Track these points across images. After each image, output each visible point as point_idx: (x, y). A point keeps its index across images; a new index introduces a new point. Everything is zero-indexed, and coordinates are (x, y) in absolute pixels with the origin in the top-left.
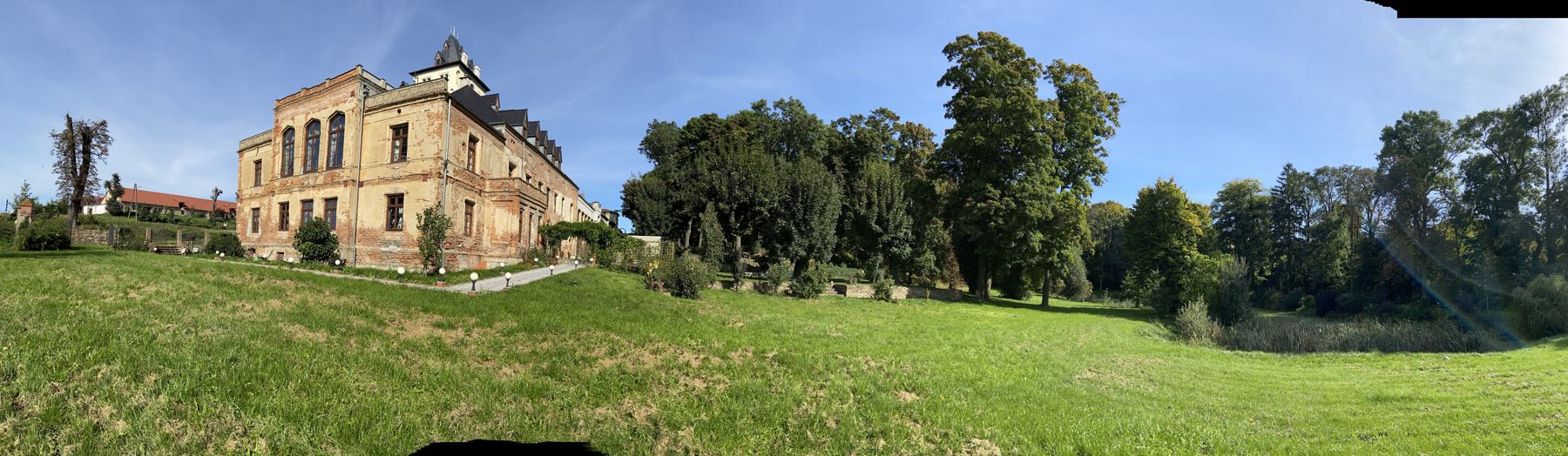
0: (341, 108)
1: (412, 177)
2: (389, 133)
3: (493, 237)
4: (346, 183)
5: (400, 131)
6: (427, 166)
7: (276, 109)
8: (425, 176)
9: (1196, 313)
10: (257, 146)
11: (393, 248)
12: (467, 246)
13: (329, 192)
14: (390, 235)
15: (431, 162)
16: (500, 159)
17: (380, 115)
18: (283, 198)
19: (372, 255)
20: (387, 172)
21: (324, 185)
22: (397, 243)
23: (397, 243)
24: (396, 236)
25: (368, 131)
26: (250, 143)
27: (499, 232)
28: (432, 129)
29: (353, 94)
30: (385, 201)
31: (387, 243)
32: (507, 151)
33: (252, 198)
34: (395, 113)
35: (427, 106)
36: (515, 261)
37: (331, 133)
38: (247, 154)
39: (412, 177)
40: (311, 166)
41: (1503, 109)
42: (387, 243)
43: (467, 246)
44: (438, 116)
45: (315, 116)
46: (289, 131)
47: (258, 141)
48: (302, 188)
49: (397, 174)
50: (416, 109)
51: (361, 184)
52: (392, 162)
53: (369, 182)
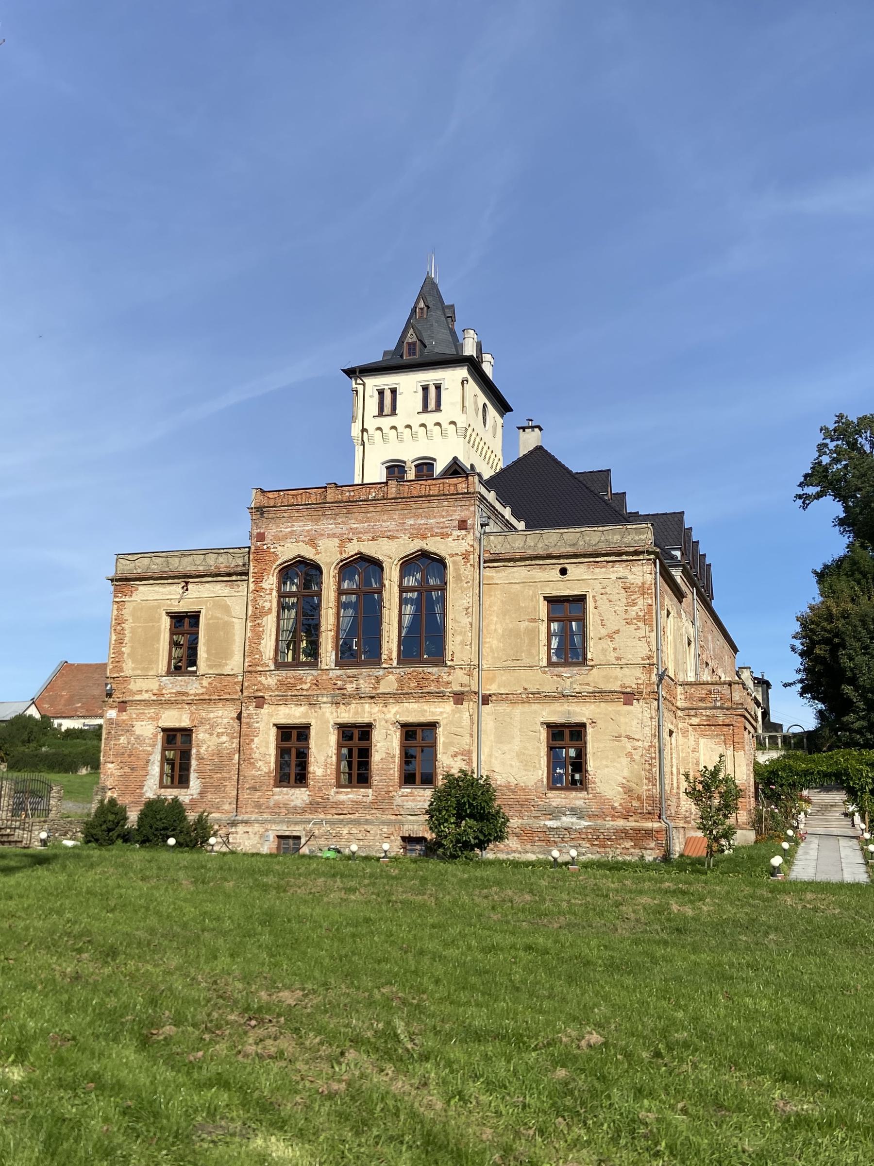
0: (434, 546)
1: (600, 695)
4: (459, 698)
6: (632, 678)
7: (260, 510)
8: (629, 697)
10: (186, 578)
11: (567, 820)
13: (415, 711)
14: (557, 799)
15: (638, 672)
17: (519, 573)
18: (293, 714)
20: (548, 682)
21: (399, 696)
22: (575, 812)
23: (575, 812)
24: (577, 798)
25: (494, 601)
26: (156, 566)
28: (633, 611)
29: (462, 525)
30: (543, 734)
31: (555, 813)
33: (161, 702)
34: (555, 573)
35: (620, 570)
38: (145, 593)
39: (600, 695)
41: (8, 718)
42: (555, 813)
44: (643, 590)
45: (370, 549)
46: (303, 572)
47: (186, 565)
48: (341, 698)
49: (567, 686)
51: (486, 700)
52: (550, 664)
53: (504, 698)
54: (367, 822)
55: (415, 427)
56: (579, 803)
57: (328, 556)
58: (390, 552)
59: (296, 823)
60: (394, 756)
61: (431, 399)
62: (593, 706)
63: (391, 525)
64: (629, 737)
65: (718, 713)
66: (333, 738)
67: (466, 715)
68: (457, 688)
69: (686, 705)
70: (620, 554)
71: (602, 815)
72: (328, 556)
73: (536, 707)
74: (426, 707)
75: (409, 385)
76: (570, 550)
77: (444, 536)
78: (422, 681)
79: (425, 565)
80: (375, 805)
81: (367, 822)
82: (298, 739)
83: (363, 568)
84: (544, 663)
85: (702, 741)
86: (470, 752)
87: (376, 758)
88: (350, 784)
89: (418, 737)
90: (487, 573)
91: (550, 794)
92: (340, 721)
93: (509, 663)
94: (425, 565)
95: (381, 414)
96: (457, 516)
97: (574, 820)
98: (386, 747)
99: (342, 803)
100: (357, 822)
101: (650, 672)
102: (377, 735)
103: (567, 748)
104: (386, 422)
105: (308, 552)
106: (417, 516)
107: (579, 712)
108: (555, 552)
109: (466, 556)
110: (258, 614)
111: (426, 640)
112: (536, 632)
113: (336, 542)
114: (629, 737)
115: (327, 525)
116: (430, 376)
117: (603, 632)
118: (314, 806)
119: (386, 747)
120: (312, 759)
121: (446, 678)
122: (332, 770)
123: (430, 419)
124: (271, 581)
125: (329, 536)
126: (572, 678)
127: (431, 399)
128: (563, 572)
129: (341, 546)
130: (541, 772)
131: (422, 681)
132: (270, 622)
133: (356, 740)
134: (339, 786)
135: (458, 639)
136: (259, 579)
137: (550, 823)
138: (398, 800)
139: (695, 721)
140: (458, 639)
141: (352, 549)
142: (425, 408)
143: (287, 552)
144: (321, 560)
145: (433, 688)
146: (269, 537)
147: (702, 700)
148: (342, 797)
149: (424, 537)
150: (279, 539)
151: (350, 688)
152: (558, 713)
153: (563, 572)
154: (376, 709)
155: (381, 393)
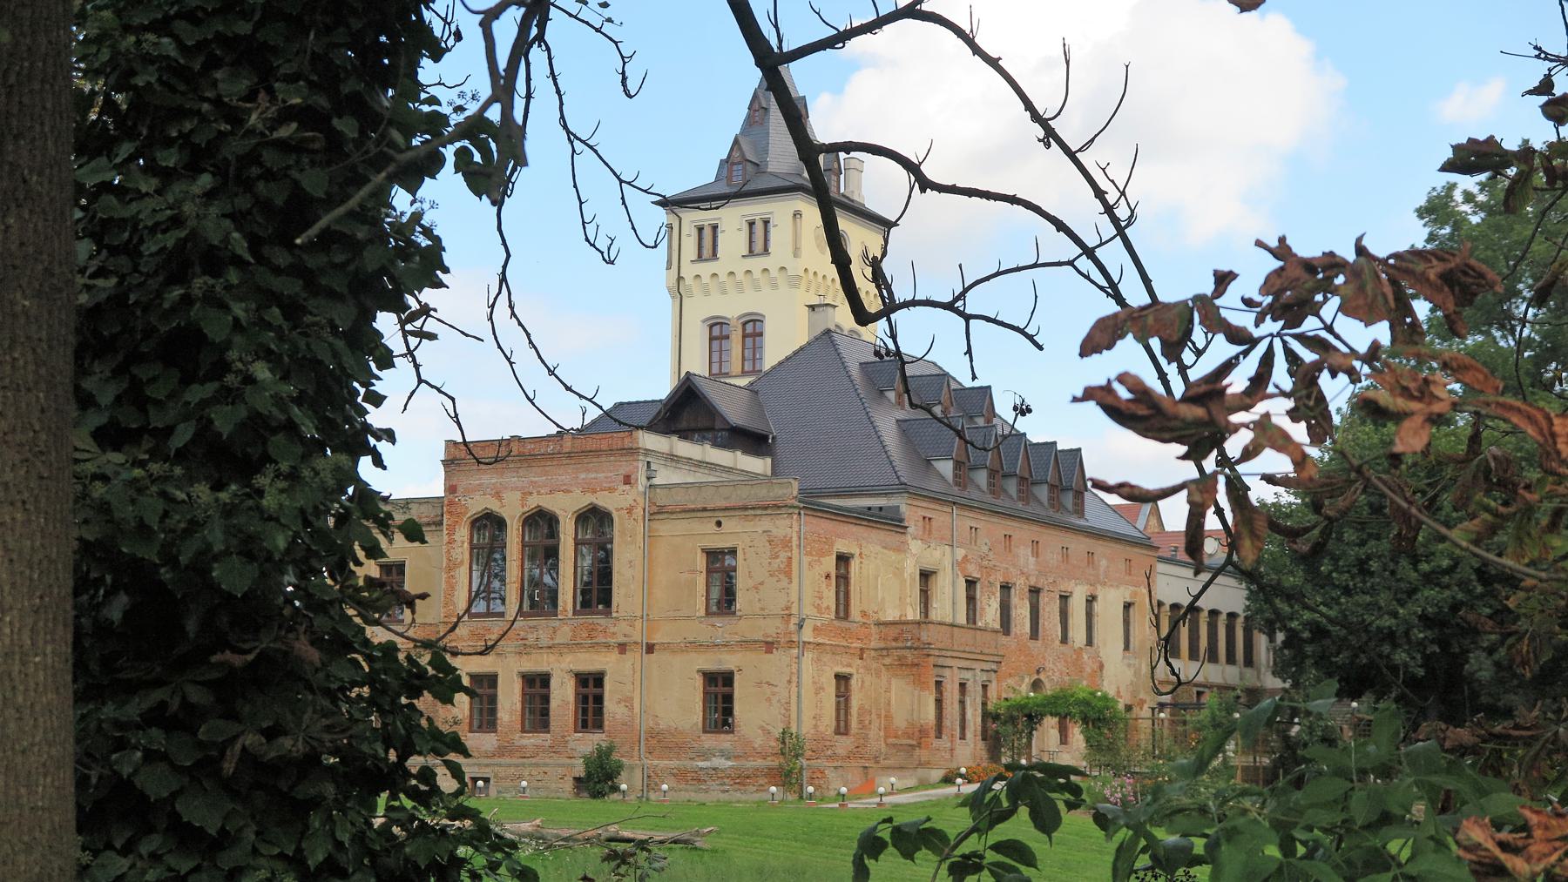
0: (604, 501)
1: (746, 644)
2: (701, 562)
3: (889, 731)
5: (719, 563)
9: (885, 833)
11: (719, 762)
12: (841, 752)
13: (589, 662)
14: (710, 741)
16: (898, 572)
19: (680, 775)
24: (724, 741)
27: (900, 722)
29: (627, 480)
30: (699, 681)
31: (704, 755)
32: (915, 546)
34: (712, 527)
36: (990, 707)
37: (577, 543)
39: (746, 644)
40: (541, 601)
43: (841, 752)
46: (490, 523)
48: (525, 649)
50: (749, 526)
51: (650, 649)
52: (708, 613)
53: (666, 647)
54: (546, 765)
55: (740, 276)
56: (727, 745)
57: (512, 510)
58: (565, 506)
59: (487, 765)
60: (1500, 555)
61: (758, 240)
62: (740, 655)
63: (565, 478)
64: (769, 684)
65: (907, 653)
66: (517, 686)
67: (628, 665)
68: (622, 639)
69: (882, 645)
70: (766, 508)
71: (745, 756)
72: (512, 510)
73: (693, 655)
74: (595, 657)
75: (732, 220)
76: (723, 504)
77: (611, 490)
78: (591, 632)
79: (595, 519)
80: (554, 750)
81: (546, 765)
82: (88, 777)
83: (541, 522)
84: (702, 612)
85: (894, 681)
86: (632, 699)
87: (554, 704)
88: (534, 730)
89: (590, 686)
90: (656, 525)
91: (704, 737)
92: (523, 669)
93: (671, 614)
94: (595, 519)
95: (700, 258)
96: (623, 471)
97: (723, 761)
98: (563, 694)
99: (525, 747)
100: (537, 765)
101: (788, 622)
102: (554, 683)
103: (719, 692)
104: (706, 269)
105: (494, 506)
106: (588, 471)
107: (728, 661)
108: (709, 506)
109: (630, 510)
110: (452, 567)
111: (597, 592)
112: (693, 583)
113: (518, 495)
114: (769, 684)
115: (511, 479)
116: (756, 209)
117: (751, 583)
118: (502, 751)
119: (563, 694)
120: (499, 706)
121: (612, 630)
122: (517, 717)
123: (756, 264)
124: (463, 533)
125: (513, 489)
126: (723, 628)
127: (758, 240)
128: (719, 524)
129: (523, 499)
130: (697, 716)
131: (591, 632)
132: (462, 573)
133: (537, 684)
134: (523, 731)
135: (623, 591)
136: (451, 532)
137: (701, 764)
138: (571, 745)
139: (887, 661)
140: (623, 591)
141: (533, 502)
142: (751, 253)
143: (477, 504)
144: (504, 514)
145: (601, 639)
146: (460, 490)
147: (896, 640)
148: (525, 742)
149: (594, 491)
150: (469, 491)
151: (531, 638)
152: (712, 662)
153: (719, 524)
154: (552, 658)
155: (700, 230)
